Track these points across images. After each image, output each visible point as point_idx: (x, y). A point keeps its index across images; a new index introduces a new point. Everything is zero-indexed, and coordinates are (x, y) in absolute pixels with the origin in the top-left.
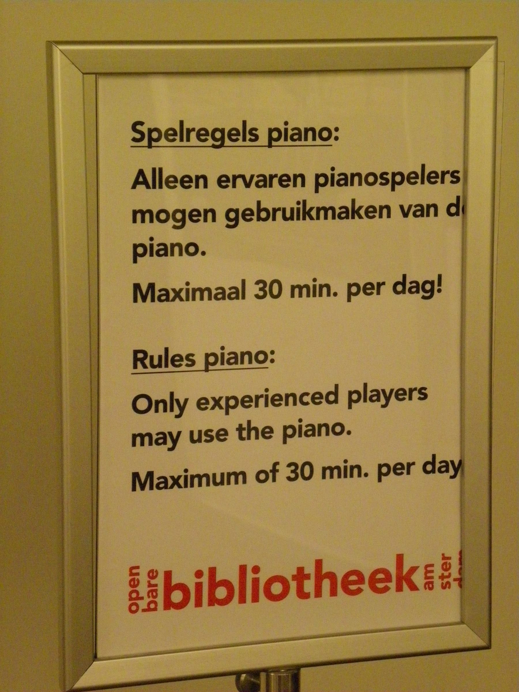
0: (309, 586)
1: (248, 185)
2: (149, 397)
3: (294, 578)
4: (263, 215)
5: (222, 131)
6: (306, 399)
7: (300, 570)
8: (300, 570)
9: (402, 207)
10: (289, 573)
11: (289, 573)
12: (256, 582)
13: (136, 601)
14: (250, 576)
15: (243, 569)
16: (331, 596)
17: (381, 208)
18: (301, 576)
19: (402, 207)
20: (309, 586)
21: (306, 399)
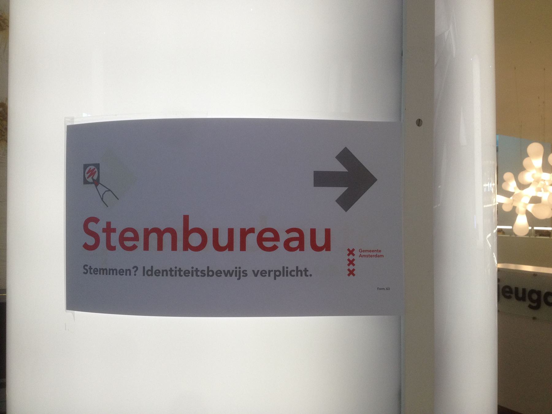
0: (173, 273)
1: (226, 275)
2: (132, 229)
3: (104, 230)
4: (211, 273)
5: (208, 275)
6: (293, 273)
7: (171, 269)
8: (171, 269)
9: (253, 271)
10: (168, 269)
11: (168, 269)
12: (287, 271)
13: (154, 271)
14: (285, 269)
15: (283, 267)
16: (188, 216)
17: (126, 270)
18: (171, 270)
19: (253, 271)
20: (173, 273)
21: (293, 273)
